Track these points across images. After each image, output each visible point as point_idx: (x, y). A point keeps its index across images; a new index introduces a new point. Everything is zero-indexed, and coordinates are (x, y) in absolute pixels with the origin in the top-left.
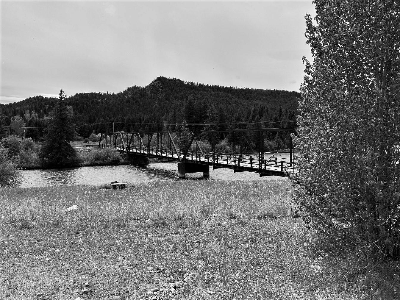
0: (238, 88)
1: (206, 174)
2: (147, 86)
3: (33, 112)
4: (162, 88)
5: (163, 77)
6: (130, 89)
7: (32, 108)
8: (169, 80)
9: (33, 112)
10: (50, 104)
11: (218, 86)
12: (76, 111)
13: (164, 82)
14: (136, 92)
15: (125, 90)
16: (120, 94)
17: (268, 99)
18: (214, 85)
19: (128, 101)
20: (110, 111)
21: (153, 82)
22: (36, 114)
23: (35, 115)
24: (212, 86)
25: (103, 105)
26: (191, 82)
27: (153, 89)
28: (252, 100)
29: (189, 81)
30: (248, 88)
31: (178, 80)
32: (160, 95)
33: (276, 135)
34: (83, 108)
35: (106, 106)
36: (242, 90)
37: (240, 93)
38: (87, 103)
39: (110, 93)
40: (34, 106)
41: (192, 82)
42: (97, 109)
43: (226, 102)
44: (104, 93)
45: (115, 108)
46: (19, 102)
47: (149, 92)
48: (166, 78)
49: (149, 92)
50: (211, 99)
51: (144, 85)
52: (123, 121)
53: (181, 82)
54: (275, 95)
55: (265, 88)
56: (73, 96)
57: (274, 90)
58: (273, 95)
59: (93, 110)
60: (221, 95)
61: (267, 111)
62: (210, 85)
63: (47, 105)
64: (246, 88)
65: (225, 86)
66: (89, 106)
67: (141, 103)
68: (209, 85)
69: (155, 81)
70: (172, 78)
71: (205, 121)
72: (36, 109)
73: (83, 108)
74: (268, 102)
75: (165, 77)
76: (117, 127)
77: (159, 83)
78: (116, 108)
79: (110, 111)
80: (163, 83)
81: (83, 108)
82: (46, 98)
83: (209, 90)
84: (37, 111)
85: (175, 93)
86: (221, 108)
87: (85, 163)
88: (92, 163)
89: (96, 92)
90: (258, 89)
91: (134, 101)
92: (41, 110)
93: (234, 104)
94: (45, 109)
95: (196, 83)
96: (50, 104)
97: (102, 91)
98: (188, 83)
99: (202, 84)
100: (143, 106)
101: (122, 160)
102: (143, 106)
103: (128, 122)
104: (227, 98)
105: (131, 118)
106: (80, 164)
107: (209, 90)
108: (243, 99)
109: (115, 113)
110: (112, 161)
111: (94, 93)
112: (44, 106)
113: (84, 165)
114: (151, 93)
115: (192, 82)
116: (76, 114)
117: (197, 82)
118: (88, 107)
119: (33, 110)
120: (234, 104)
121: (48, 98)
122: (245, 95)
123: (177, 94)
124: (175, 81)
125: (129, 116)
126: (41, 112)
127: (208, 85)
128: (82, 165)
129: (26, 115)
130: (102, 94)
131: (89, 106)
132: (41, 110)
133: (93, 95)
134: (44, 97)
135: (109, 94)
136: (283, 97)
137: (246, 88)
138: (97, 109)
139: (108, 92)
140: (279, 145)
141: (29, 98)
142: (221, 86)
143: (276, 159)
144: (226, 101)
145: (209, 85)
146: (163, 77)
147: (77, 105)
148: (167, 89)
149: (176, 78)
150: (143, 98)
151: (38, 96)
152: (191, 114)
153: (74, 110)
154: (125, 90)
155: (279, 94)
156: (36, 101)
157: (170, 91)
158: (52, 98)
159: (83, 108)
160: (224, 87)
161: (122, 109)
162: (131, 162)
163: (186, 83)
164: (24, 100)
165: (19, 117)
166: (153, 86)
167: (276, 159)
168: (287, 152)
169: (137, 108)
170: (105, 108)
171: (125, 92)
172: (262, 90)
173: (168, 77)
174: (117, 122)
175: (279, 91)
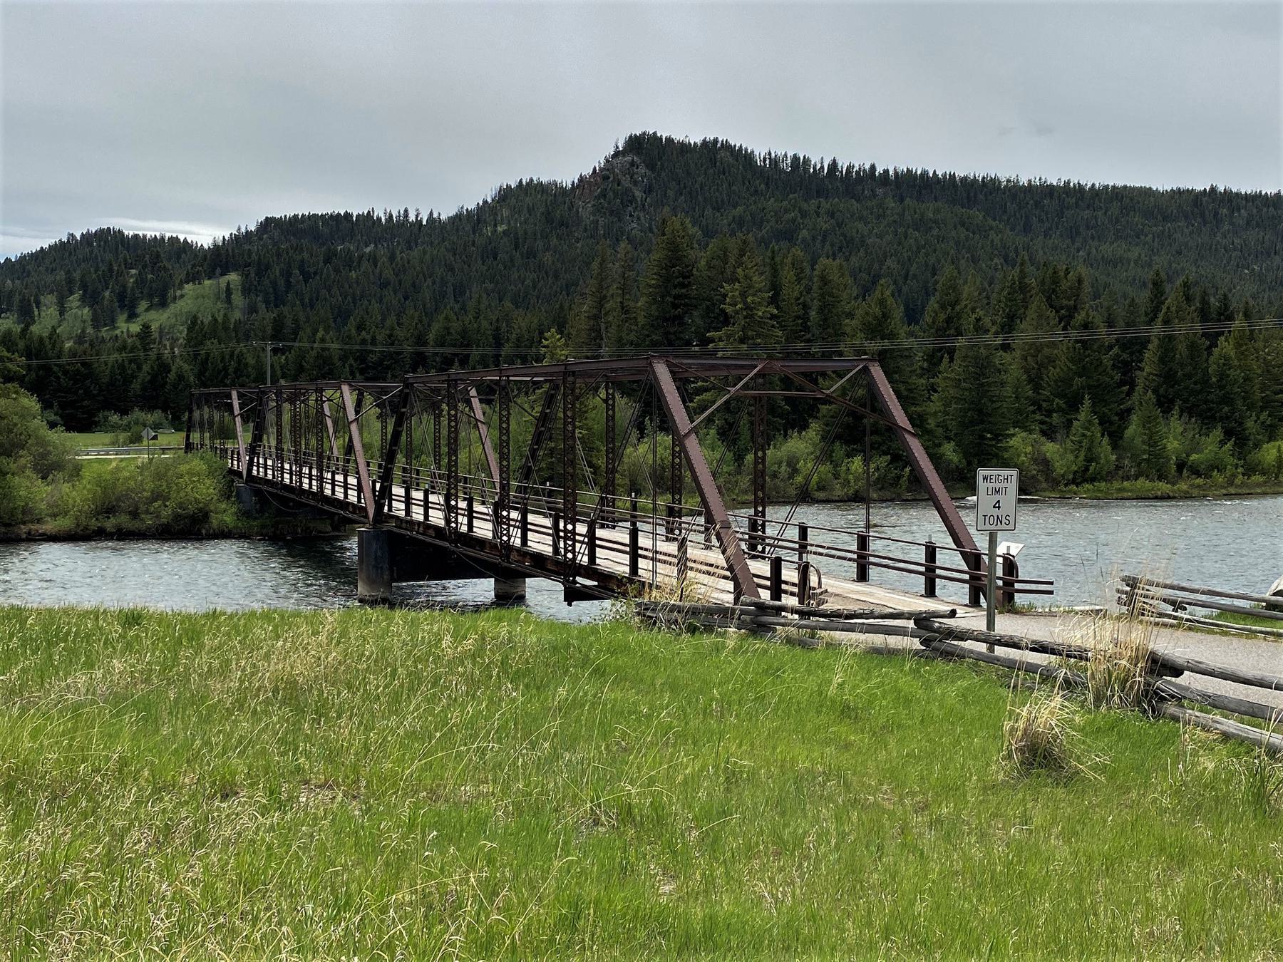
0: (1024, 181)
1: (506, 588)
2: (581, 179)
3: (74, 300)
4: (649, 190)
5: (655, 133)
6: (505, 195)
7: (70, 281)
8: (684, 148)
9: (74, 300)
10: (145, 267)
11: (924, 173)
12: (257, 296)
13: (660, 159)
14: (530, 210)
15: (485, 202)
16: (458, 218)
17: (1178, 235)
18: (903, 168)
19: (490, 253)
20: (406, 298)
21: (607, 161)
22: (86, 310)
23: (78, 311)
24: (896, 173)
25: (377, 271)
26: (790, 154)
27: (604, 195)
28: (1093, 238)
29: (781, 153)
30: (1074, 181)
31: (727, 147)
32: (639, 218)
33: (1077, 410)
34: (288, 281)
35: (388, 273)
36: (1049, 191)
37: (1037, 204)
38: (302, 261)
39: (417, 216)
40: (77, 275)
41: (795, 158)
42: (347, 286)
43: (952, 252)
44: (391, 216)
45: (429, 281)
46: (23, 258)
47: (585, 210)
48: (669, 140)
49: (585, 210)
50: (880, 236)
51: (567, 176)
52: (420, 340)
53: (743, 158)
54: (1216, 214)
55: (1163, 182)
56: (252, 228)
57: (1213, 189)
58: (1202, 215)
59: (329, 291)
60: (931, 215)
61: (267, 302)
62: (886, 171)
63: (133, 271)
64: (1069, 182)
65: (960, 173)
66: (315, 273)
67: (548, 258)
68: (879, 170)
69: (617, 154)
70: (696, 138)
71: (712, 340)
72: (84, 286)
73: (288, 285)
74: (1179, 253)
75: (663, 133)
76: (388, 367)
77: (632, 164)
78: (434, 283)
79: (406, 298)
80: (651, 166)
81: (288, 285)
82: (136, 236)
83: (880, 191)
84: (91, 298)
85: (709, 212)
86: (824, 280)
87: (49, 526)
88: (78, 525)
89: (357, 209)
90: (1125, 187)
91: (517, 247)
92: (107, 294)
93: (996, 260)
94: (124, 287)
95: (815, 160)
96: (145, 267)
97: (383, 205)
98: (775, 162)
99: (843, 164)
100: (556, 277)
101: (226, 515)
102: (556, 277)
103: (442, 345)
104: (963, 233)
105: (456, 326)
106: (24, 529)
107: (880, 191)
108: (1046, 234)
109: (429, 305)
110: (177, 517)
111: (348, 216)
112: (120, 274)
113: (40, 535)
114: (598, 209)
115: (795, 158)
116: (252, 309)
117: (819, 155)
118: (307, 277)
119: (71, 293)
120: (996, 260)
121: (145, 236)
122: (1061, 214)
123: (718, 214)
124: (711, 149)
125: (446, 318)
126: (106, 302)
127: (873, 167)
128: (29, 533)
129: (43, 314)
130: (379, 219)
131: (315, 273)
132: (107, 294)
133: (339, 223)
134: (129, 233)
135: (412, 218)
136: (1258, 225)
137: (1069, 182)
138: (347, 286)
139: (406, 211)
140: (1090, 460)
141: (65, 240)
142: (940, 173)
143: (803, 531)
144: (957, 243)
145: (879, 170)
146: (655, 133)
147: (263, 268)
148: (671, 193)
149: (716, 141)
150: (559, 238)
151: (102, 230)
152: (675, 306)
153: (246, 291)
154: (485, 202)
155: (1239, 210)
156: (96, 251)
157: (686, 202)
158: (163, 238)
159: (288, 281)
160: (953, 177)
161: (460, 291)
162: (264, 526)
163: (765, 159)
164: (46, 246)
165: (14, 323)
166: (606, 178)
167: (803, 531)
168: (1125, 495)
169: (528, 282)
170: (384, 285)
171: (484, 208)
172: (1147, 193)
173: (678, 137)
174: (392, 344)
175: (1238, 194)
